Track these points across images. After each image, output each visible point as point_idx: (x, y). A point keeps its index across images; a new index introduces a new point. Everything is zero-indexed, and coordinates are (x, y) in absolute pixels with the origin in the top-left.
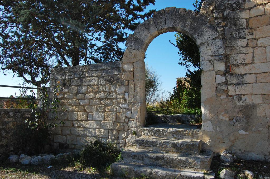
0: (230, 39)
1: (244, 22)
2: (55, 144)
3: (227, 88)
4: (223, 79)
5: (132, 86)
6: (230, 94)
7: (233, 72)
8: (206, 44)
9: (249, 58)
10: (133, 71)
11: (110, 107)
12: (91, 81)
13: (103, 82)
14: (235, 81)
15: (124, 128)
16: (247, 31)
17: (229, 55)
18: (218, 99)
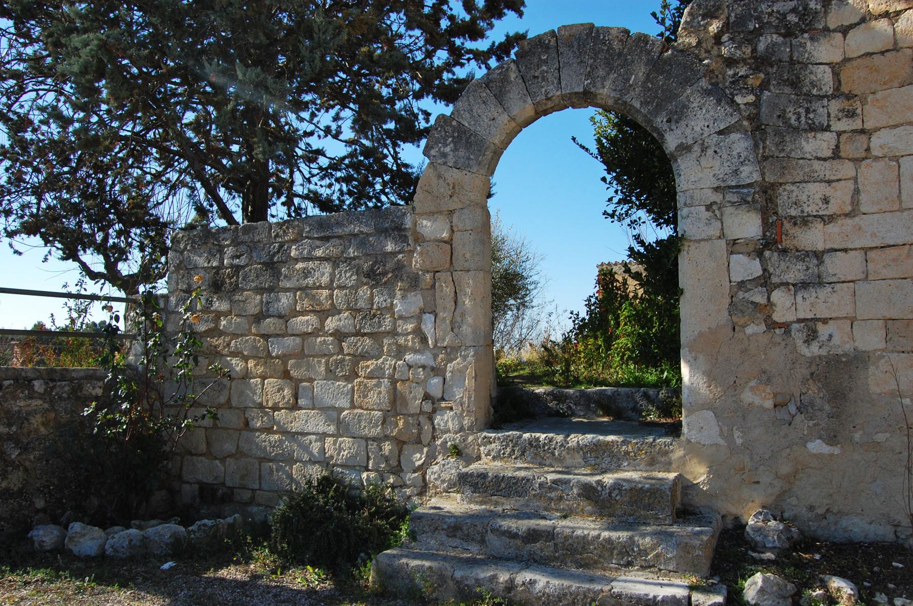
1: (825, 76)
2: (186, 487)
3: (769, 298)
4: (755, 268)
5: (448, 290)
8: (697, 148)
9: (840, 197)
10: (449, 242)
11: (372, 364)
12: (306, 273)
13: (348, 278)
14: (795, 272)
16: (835, 106)
17: (773, 186)
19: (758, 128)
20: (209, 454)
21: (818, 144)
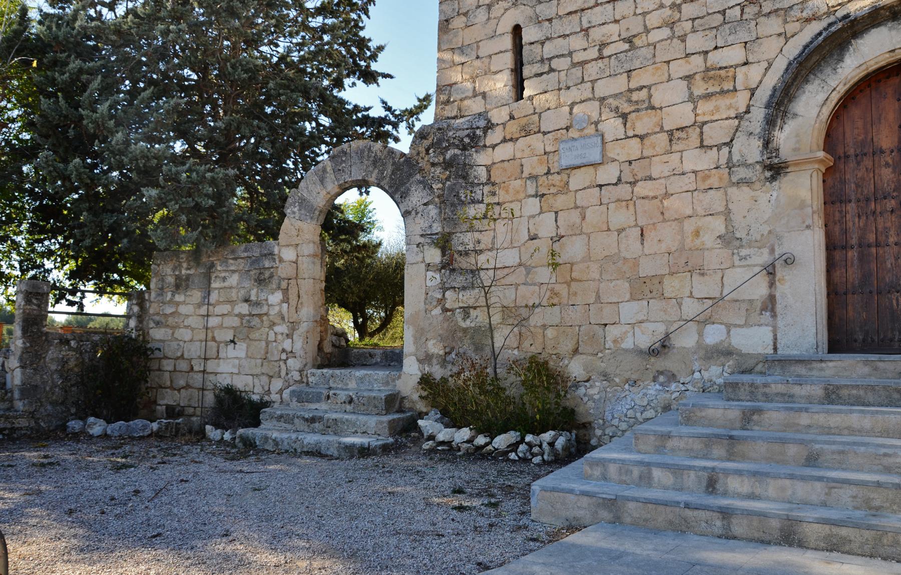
0: (453, 205)
1: (482, 173)
2: (159, 408)
3: (444, 295)
6: (447, 306)
7: (456, 265)
8: (413, 213)
10: (296, 262)
15: (280, 371)
16: (487, 189)
17: (450, 234)
18: (429, 315)
19: (443, 202)
20: (172, 388)
21: (472, 211)
